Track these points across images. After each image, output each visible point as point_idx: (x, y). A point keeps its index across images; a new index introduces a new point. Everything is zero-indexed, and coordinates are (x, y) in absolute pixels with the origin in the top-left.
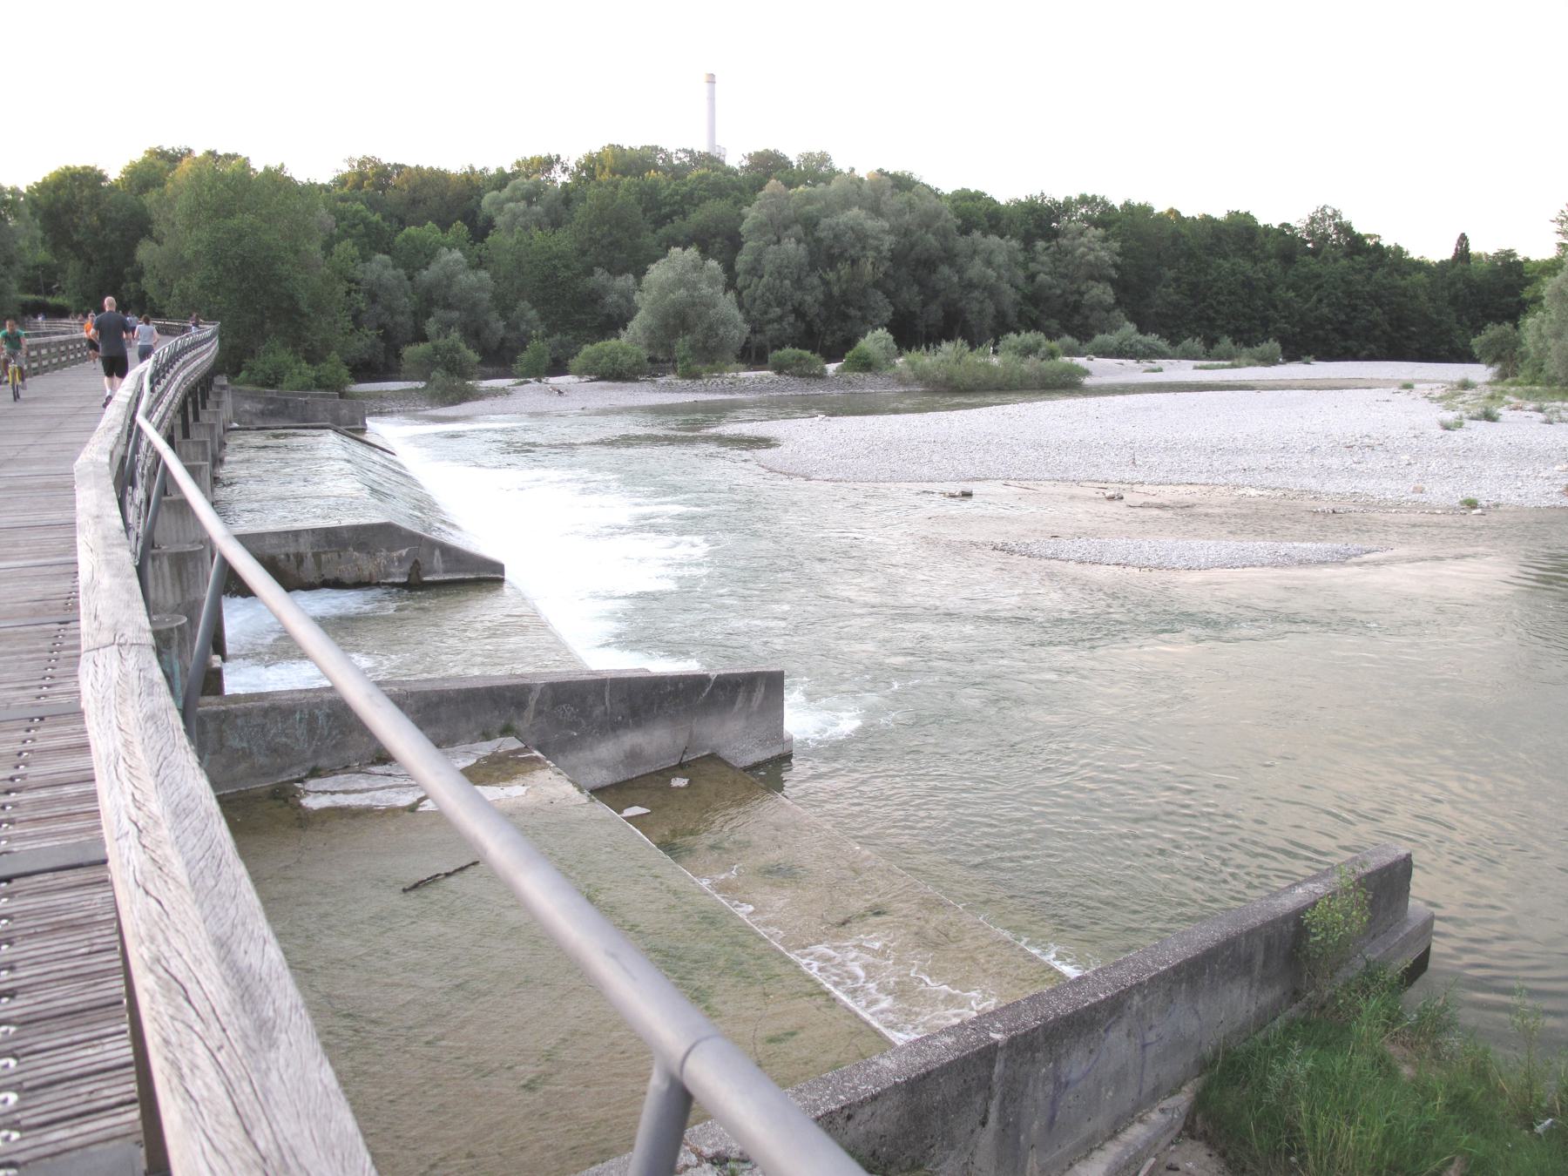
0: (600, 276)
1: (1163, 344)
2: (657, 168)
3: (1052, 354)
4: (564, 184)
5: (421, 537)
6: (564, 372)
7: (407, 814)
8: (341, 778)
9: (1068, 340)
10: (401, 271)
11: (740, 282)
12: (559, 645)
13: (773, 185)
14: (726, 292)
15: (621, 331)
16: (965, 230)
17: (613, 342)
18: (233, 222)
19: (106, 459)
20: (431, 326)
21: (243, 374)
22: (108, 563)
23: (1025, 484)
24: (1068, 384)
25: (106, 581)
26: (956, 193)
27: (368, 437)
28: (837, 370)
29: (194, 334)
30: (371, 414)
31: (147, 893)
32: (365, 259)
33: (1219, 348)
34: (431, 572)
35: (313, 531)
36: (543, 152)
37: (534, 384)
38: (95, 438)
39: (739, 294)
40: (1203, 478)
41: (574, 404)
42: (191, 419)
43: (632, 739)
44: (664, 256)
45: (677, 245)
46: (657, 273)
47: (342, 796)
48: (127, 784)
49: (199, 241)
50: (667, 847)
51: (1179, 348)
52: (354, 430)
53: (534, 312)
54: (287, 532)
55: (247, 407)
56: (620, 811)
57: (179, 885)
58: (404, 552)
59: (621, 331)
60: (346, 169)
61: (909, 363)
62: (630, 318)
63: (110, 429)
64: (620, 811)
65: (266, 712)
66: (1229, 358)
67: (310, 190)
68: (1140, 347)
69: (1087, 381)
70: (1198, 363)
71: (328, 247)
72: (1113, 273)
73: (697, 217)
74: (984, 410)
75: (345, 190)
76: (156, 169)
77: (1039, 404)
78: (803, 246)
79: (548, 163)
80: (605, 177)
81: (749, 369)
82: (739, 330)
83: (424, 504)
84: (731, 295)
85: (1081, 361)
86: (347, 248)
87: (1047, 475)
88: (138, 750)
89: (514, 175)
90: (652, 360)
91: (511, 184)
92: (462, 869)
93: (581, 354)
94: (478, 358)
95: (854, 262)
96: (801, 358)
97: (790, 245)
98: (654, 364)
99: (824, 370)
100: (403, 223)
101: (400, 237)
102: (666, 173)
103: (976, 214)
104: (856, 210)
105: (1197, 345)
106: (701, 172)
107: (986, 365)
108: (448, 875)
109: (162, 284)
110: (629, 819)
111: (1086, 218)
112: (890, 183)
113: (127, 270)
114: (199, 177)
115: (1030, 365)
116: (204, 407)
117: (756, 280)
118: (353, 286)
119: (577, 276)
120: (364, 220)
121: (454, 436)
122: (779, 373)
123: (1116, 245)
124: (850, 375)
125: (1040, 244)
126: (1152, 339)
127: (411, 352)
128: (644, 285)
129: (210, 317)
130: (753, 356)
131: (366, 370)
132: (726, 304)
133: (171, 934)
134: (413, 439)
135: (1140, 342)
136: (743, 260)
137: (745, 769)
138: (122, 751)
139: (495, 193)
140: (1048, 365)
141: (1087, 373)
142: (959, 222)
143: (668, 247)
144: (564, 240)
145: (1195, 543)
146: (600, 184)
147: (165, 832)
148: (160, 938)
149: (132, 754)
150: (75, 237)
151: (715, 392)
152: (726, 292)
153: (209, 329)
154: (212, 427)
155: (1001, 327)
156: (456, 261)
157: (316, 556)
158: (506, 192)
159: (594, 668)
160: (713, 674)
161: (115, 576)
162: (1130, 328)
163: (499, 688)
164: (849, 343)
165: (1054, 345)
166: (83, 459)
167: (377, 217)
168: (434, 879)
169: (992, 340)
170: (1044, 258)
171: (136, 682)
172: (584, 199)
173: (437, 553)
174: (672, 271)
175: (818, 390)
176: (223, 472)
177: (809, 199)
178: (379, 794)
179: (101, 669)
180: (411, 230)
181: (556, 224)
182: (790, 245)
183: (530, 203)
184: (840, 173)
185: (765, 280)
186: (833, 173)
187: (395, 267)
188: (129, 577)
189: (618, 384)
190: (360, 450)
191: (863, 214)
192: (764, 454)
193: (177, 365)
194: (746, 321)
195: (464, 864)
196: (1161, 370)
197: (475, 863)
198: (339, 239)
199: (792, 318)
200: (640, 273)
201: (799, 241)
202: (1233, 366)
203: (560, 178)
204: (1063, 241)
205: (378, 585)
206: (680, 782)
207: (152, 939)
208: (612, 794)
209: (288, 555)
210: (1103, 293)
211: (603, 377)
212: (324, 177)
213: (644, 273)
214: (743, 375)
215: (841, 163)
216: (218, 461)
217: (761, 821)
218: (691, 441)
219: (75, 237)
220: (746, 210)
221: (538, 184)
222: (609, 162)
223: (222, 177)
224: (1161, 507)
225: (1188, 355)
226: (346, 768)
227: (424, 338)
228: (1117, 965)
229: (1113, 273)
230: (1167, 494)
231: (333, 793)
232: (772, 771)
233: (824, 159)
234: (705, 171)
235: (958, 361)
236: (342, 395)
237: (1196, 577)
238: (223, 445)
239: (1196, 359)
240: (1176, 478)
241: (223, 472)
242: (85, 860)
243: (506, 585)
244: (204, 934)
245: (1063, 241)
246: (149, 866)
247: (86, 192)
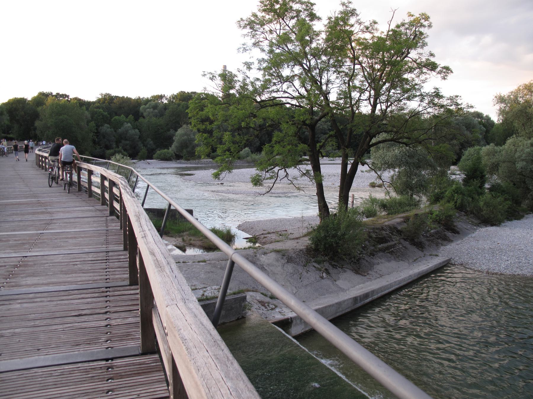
6: (152, 159)
10: (112, 129)
17: (166, 150)
18: (61, 117)
36: (156, 94)
37: (143, 161)
46: (180, 131)
49: (52, 122)
60: (100, 97)
76: (42, 98)
79: (161, 97)
91: (149, 103)
98: (178, 157)
101: (112, 120)
109: (42, 132)
113: (32, 128)
114: (53, 105)
119: (165, 131)
120: (102, 114)
139: (144, 106)
144: (161, 121)
150: (17, 118)
156: (129, 127)
158: (148, 105)
167: (106, 113)
198: (91, 121)
219: (17, 118)
222: (179, 97)
223: (59, 105)
247: (21, 105)
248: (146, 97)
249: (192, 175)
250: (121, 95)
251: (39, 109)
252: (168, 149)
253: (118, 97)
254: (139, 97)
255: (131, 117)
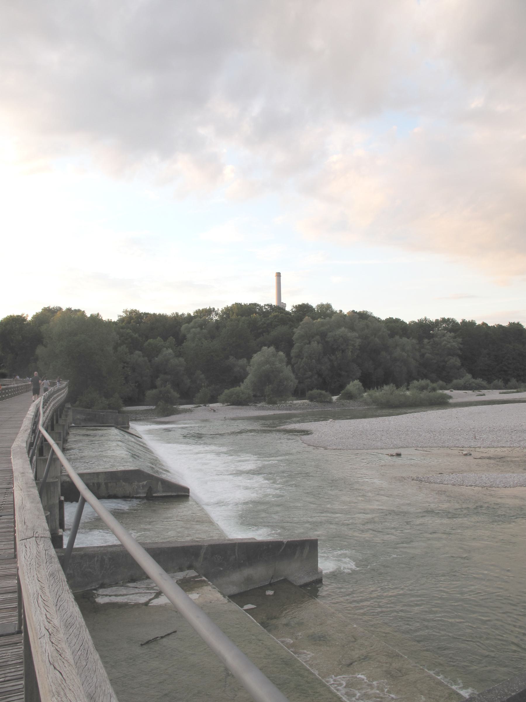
0: (232, 360)
1: (484, 383)
2: (256, 313)
3: (434, 389)
4: (216, 320)
5: (153, 476)
6: (216, 402)
7: (144, 606)
8: (114, 588)
9: (441, 382)
10: (146, 358)
11: (293, 361)
12: (221, 533)
13: (307, 319)
14: (287, 365)
15: (241, 383)
16: (392, 336)
17: (238, 388)
19: (24, 445)
20: (158, 382)
21: (77, 403)
22: (29, 496)
23: (425, 449)
24: (442, 403)
25: (28, 505)
26: (387, 320)
27: (130, 430)
28: (337, 399)
29: (58, 386)
30: (132, 420)
31: (55, 668)
32: (131, 353)
33: (510, 384)
34: (157, 492)
35: (105, 473)
37: (203, 407)
38: (19, 435)
39: (293, 366)
40: (508, 444)
41: (219, 415)
42: (55, 422)
43: (248, 572)
44: (260, 351)
45: (265, 346)
46: (257, 358)
47: (114, 597)
48: (43, 609)
50: (263, 624)
51: (492, 385)
52: (124, 427)
53: (203, 375)
54: (94, 473)
55: (78, 417)
56: (242, 607)
57: (70, 665)
58: (145, 483)
59: (241, 383)
60: (124, 315)
61: (369, 395)
62: (245, 378)
63: (26, 430)
64: (242, 607)
65: (82, 557)
66: (515, 388)
67: (110, 323)
68: (474, 385)
69: (451, 401)
70: (501, 391)
71: (115, 348)
72: (460, 352)
73: (274, 333)
74: (404, 416)
75: (124, 324)
76: (48, 315)
77: (429, 412)
78: (320, 345)
79: (209, 312)
80: (234, 317)
81: (297, 399)
82: (293, 383)
83: (155, 461)
84: (289, 367)
85: (447, 392)
86: (123, 348)
87: (435, 445)
88: (47, 591)
89: (195, 317)
90: (255, 396)
91: (194, 321)
92: (168, 635)
93: (224, 394)
94: (178, 396)
95: (343, 351)
96: (321, 394)
97: (314, 344)
99: (331, 399)
100: (147, 338)
101: (146, 344)
102: (260, 315)
103: (395, 326)
104: (343, 329)
105: (500, 383)
106: (275, 314)
107: (404, 395)
108: (162, 637)
110: (246, 610)
111: (445, 329)
112: (358, 317)
115: (424, 394)
116: (61, 417)
117: (300, 360)
118: (125, 365)
121: (168, 430)
122: (311, 401)
123: (460, 340)
124: (343, 401)
125: (426, 341)
126: (479, 381)
127: (150, 393)
128: (251, 363)
129: (65, 378)
130: (299, 394)
131: (130, 401)
132: (287, 371)
133: (67, 691)
134: (150, 432)
135: (474, 382)
136: (294, 351)
137: (301, 586)
138: (40, 592)
139: (187, 324)
140: (432, 394)
141: (450, 397)
142: (389, 332)
143: (261, 347)
145: (507, 475)
146: (231, 320)
147: (61, 635)
148: (62, 693)
149: (44, 593)
151: (282, 410)
152: (287, 365)
153: (65, 383)
154: (64, 426)
155: (410, 378)
157: (106, 484)
158: (192, 324)
159: (231, 537)
160: (285, 541)
161: (32, 502)
162: (469, 376)
163: (187, 547)
164: (342, 387)
165: (435, 385)
166: (15, 445)
167: (136, 335)
168: (155, 639)
169: (406, 384)
170: (428, 347)
171: (44, 556)
172: (225, 327)
173: (160, 483)
174: (264, 357)
175: (329, 408)
176: (67, 446)
177: (323, 325)
178: (131, 597)
179: (28, 549)
180: (151, 341)
181: (213, 337)
182: (314, 344)
183: (202, 329)
184: (336, 312)
185: (304, 359)
186: (333, 313)
187: (143, 356)
188: (38, 503)
189: (240, 407)
190: (127, 436)
191: (347, 330)
192: (305, 437)
193: (51, 399)
194: (296, 378)
195: (169, 632)
196: (484, 395)
197: (175, 632)
199: (316, 377)
200: (249, 358)
201: (318, 343)
202: (518, 392)
203: (215, 318)
204: (436, 339)
205: (133, 497)
206: (270, 593)
207: (59, 694)
208: (238, 598)
209: (94, 483)
210: (455, 361)
211: (233, 404)
212: (115, 319)
213: (251, 358)
214: (295, 402)
215: (336, 308)
216: (65, 441)
217: (307, 612)
218: (270, 431)
220: (295, 330)
221: (205, 320)
224: (489, 458)
225: (496, 388)
226: (116, 584)
227: (155, 387)
228: (489, 691)
229: (460, 352)
230: (492, 452)
231: (110, 596)
232: (313, 587)
233: (329, 306)
234: (277, 313)
235: (391, 394)
236: (119, 412)
237: (508, 491)
238: (68, 434)
239: (500, 389)
240: (496, 444)
241: (67, 446)
242: (5, 633)
243: (190, 498)
244: (83, 692)
245: (436, 339)
246: (55, 654)
248: (186, 313)
249: (306, 433)
250: (151, 312)
251: (44, 328)
252: (240, 386)
253: (148, 314)
254: (177, 314)
255: (171, 339)
